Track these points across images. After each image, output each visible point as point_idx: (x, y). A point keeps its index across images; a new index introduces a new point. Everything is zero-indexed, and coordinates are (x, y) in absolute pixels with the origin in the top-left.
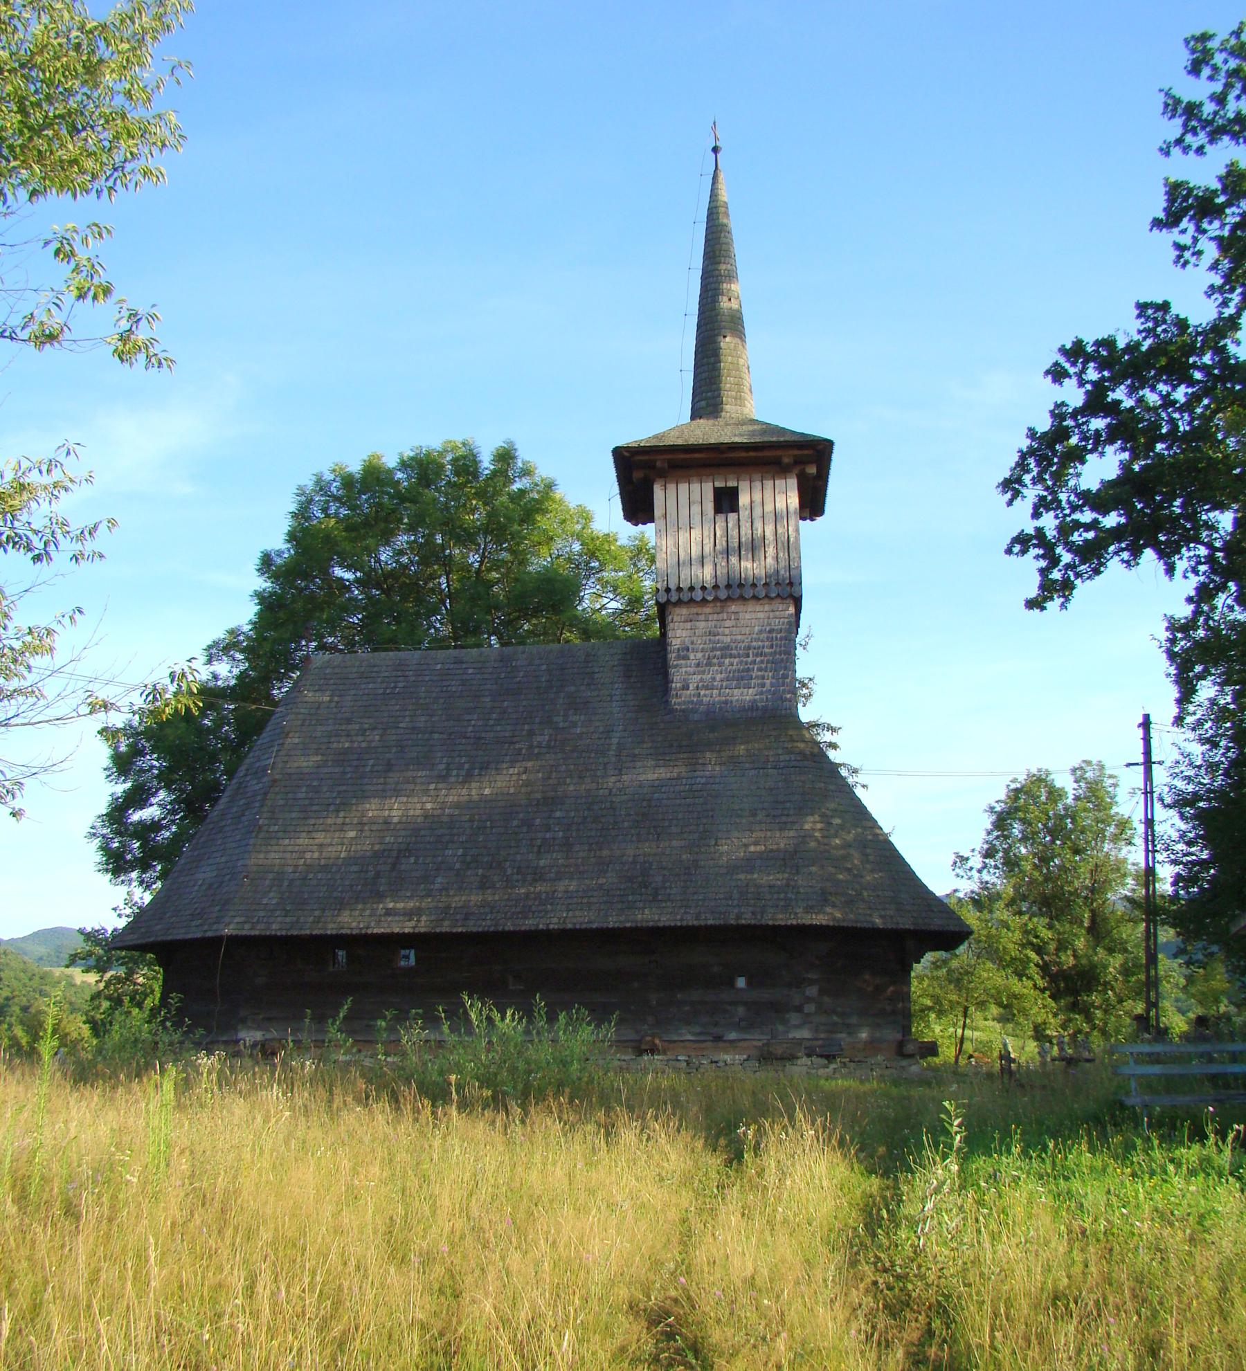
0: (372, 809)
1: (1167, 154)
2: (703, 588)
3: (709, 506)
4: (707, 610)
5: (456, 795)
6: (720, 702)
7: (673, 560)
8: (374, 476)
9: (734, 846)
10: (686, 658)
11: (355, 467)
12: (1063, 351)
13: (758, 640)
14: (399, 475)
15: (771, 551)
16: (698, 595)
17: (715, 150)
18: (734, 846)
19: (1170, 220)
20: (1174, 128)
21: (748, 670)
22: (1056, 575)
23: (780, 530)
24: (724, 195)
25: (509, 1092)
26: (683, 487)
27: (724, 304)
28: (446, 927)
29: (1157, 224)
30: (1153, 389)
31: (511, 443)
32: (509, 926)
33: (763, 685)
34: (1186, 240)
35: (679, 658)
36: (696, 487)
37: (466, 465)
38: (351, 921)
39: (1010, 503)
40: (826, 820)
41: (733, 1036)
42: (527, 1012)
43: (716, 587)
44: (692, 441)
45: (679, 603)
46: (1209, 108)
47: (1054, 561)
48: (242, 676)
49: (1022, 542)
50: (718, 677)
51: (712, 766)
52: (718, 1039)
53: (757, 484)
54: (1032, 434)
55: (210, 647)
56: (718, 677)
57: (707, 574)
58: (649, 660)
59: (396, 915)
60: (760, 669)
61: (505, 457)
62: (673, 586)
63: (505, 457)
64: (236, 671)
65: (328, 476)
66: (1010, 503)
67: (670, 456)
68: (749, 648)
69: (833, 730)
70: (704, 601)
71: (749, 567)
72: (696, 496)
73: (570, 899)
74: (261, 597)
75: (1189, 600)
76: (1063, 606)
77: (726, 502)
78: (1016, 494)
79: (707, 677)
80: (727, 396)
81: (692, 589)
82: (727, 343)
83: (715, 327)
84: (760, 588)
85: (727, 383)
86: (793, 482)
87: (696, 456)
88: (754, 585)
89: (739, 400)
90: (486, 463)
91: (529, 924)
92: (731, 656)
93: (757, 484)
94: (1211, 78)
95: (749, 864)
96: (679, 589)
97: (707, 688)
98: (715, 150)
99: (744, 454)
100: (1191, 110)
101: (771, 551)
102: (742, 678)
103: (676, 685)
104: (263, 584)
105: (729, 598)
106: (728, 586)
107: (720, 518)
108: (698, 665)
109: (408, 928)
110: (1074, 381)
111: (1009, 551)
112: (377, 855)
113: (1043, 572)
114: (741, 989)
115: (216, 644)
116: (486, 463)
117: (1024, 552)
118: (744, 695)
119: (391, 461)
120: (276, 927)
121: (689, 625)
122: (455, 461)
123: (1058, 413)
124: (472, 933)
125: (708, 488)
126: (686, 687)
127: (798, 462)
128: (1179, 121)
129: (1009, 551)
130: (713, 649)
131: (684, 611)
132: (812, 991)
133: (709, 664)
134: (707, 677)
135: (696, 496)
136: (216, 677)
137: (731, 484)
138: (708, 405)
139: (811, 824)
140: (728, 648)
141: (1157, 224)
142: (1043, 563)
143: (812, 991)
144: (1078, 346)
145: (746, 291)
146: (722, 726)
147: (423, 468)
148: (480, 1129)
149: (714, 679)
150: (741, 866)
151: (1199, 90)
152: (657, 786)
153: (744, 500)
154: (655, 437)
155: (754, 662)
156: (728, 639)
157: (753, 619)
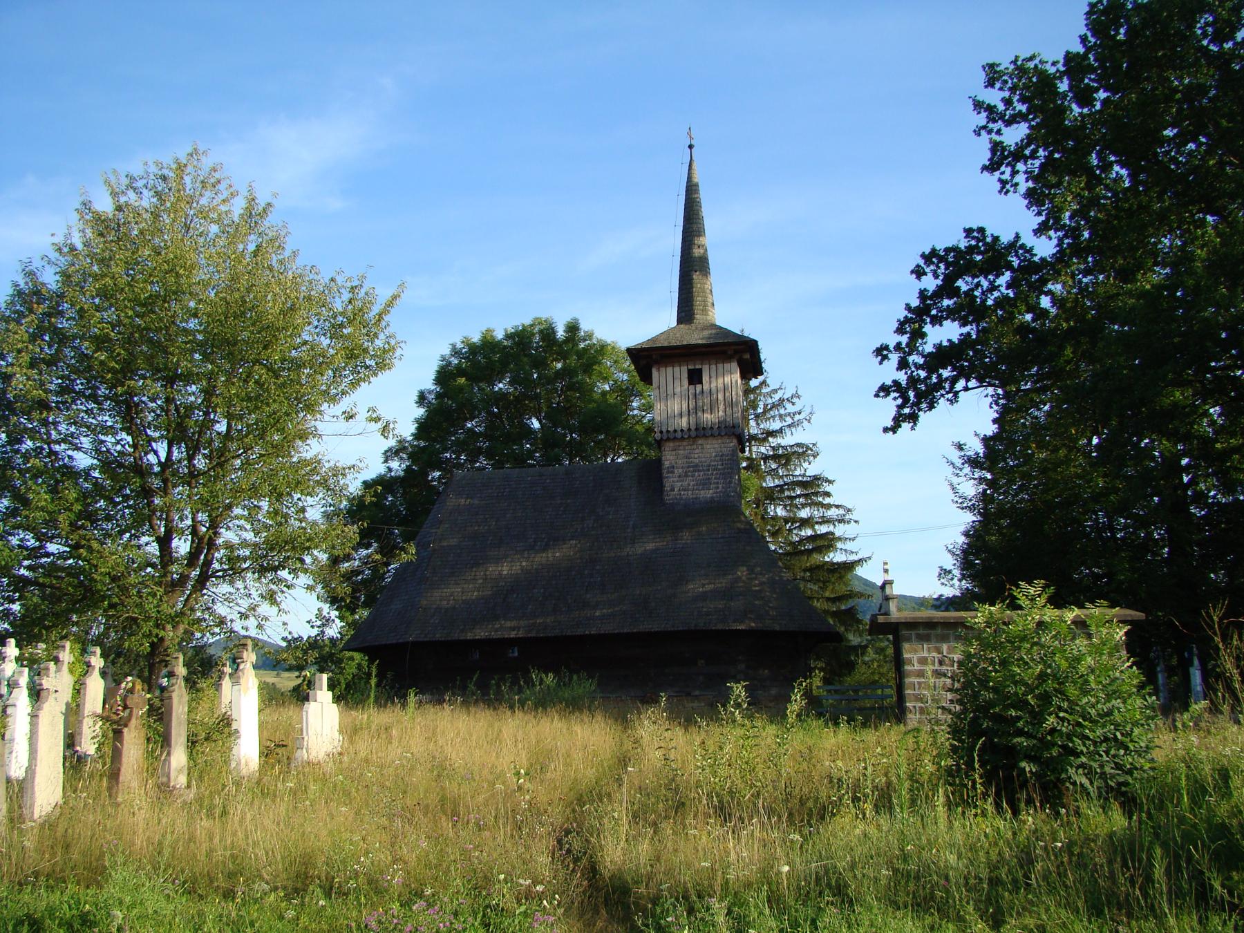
0: (492, 569)
1: (979, 135)
3: (686, 382)
5: (541, 558)
8: (488, 345)
9: (696, 587)
11: (476, 338)
12: (923, 256)
14: (506, 343)
16: (679, 435)
17: (691, 147)
18: (696, 587)
19: (992, 167)
20: (982, 119)
22: (907, 411)
24: (697, 178)
25: (543, 703)
26: (670, 370)
27: (697, 252)
28: (533, 634)
29: (985, 168)
30: (986, 278)
31: (576, 320)
32: (569, 633)
34: (1006, 176)
36: (677, 369)
37: (548, 333)
38: (480, 633)
39: (881, 363)
40: (751, 570)
41: (697, 693)
42: (557, 673)
43: (689, 429)
44: (673, 343)
45: (668, 439)
46: (1001, 107)
47: (906, 400)
48: (408, 470)
49: (884, 390)
51: (686, 537)
52: (688, 694)
53: (713, 367)
54: (908, 308)
55: (386, 452)
58: (652, 473)
59: (508, 628)
61: (573, 328)
63: (573, 328)
64: (404, 466)
65: (459, 346)
66: (881, 363)
69: (830, 482)
70: (683, 439)
71: (708, 418)
72: (677, 374)
73: (602, 615)
75: (995, 421)
76: (912, 428)
77: (695, 378)
78: (885, 357)
79: (685, 484)
80: (698, 309)
81: (675, 431)
82: (696, 276)
83: (692, 266)
85: (698, 301)
86: (734, 365)
89: (705, 312)
90: (561, 333)
91: (579, 632)
93: (713, 367)
94: (1001, 89)
95: (704, 597)
96: (668, 431)
98: (691, 147)
100: (990, 109)
101: (722, 407)
102: (705, 484)
103: (667, 488)
104: (420, 412)
105: (697, 436)
106: (697, 429)
109: (513, 635)
110: (930, 275)
111: (877, 396)
113: (900, 407)
115: (390, 450)
116: (561, 333)
117: (888, 394)
118: (707, 494)
119: (499, 335)
120: (439, 636)
122: (541, 332)
123: (922, 294)
125: (684, 369)
127: (736, 352)
128: (984, 114)
129: (877, 396)
131: (671, 444)
132: (742, 667)
133: (686, 476)
134: (685, 484)
135: (677, 374)
136: (390, 470)
137: (698, 367)
139: (742, 572)
140: (697, 466)
141: (985, 168)
142: (900, 401)
143: (742, 667)
144: (934, 252)
146: (694, 513)
147: (520, 338)
148: (529, 717)
150: (701, 595)
151: (994, 97)
152: (654, 551)
153: (705, 379)
154: (652, 340)
157: (711, 449)
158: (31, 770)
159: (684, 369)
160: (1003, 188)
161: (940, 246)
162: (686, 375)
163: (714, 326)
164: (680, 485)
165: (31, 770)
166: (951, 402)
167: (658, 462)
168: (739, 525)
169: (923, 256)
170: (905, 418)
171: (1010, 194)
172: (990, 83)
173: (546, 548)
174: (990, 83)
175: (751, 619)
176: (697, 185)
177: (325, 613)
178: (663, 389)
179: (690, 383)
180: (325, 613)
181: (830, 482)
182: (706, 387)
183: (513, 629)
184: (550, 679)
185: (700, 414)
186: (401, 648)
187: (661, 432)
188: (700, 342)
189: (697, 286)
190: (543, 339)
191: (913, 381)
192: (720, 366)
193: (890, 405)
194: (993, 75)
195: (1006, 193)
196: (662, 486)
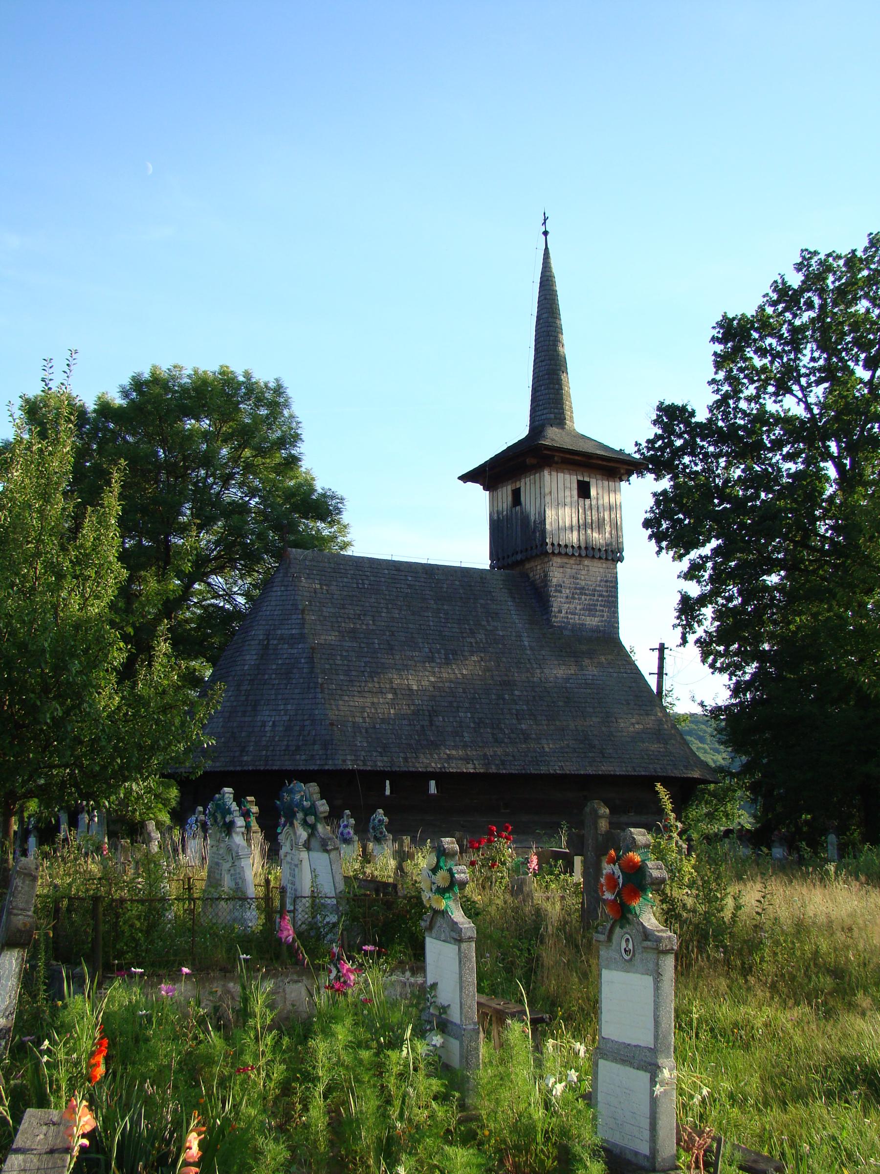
2: (572, 546)
3: (575, 493)
4: (572, 561)
5: (446, 674)
6: (580, 624)
7: (555, 526)
10: (560, 592)
13: (600, 586)
15: (608, 529)
16: (563, 551)
17: (546, 233)
21: (595, 605)
23: (613, 516)
26: (561, 475)
33: (603, 616)
35: (556, 591)
43: (579, 547)
50: (578, 607)
56: (578, 607)
57: (573, 538)
60: (601, 606)
62: (556, 543)
67: (562, 455)
68: (595, 590)
74: (323, 508)
77: (584, 491)
79: (572, 606)
81: (566, 546)
84: (603, 552)
87: (576, 458)
88: (600, 550)
92: (585, 594)
96: (559, 545)
97: (572, 614)
98: (546, 233)
99: (600, 462)
101: (608, 529)
103: (555, 609)
106: (586, 548)
107: (581, 501)
108: (567, 597)
112: (416, 713)
114: (812, 818)
118: (592, 622)
121: (561, 570)
124: (512, 774)
125: (574, 479)
126: (560, 612)
130: (576, 588)
133: (573, 598)
137: (587, 479)
138: (556, 418)
140: (583, 588)
145: (571, 346)
149: (576, 608)
155: (597, 600)
156: (583, 583)
157: (596, 569)
158: (538, 1048)
159: (574, 479)
162: (575, 485)
165: (538, 1048)
178: (554, 495)
179: (579, 496)
182: (594, 502)
187: (553, 544)
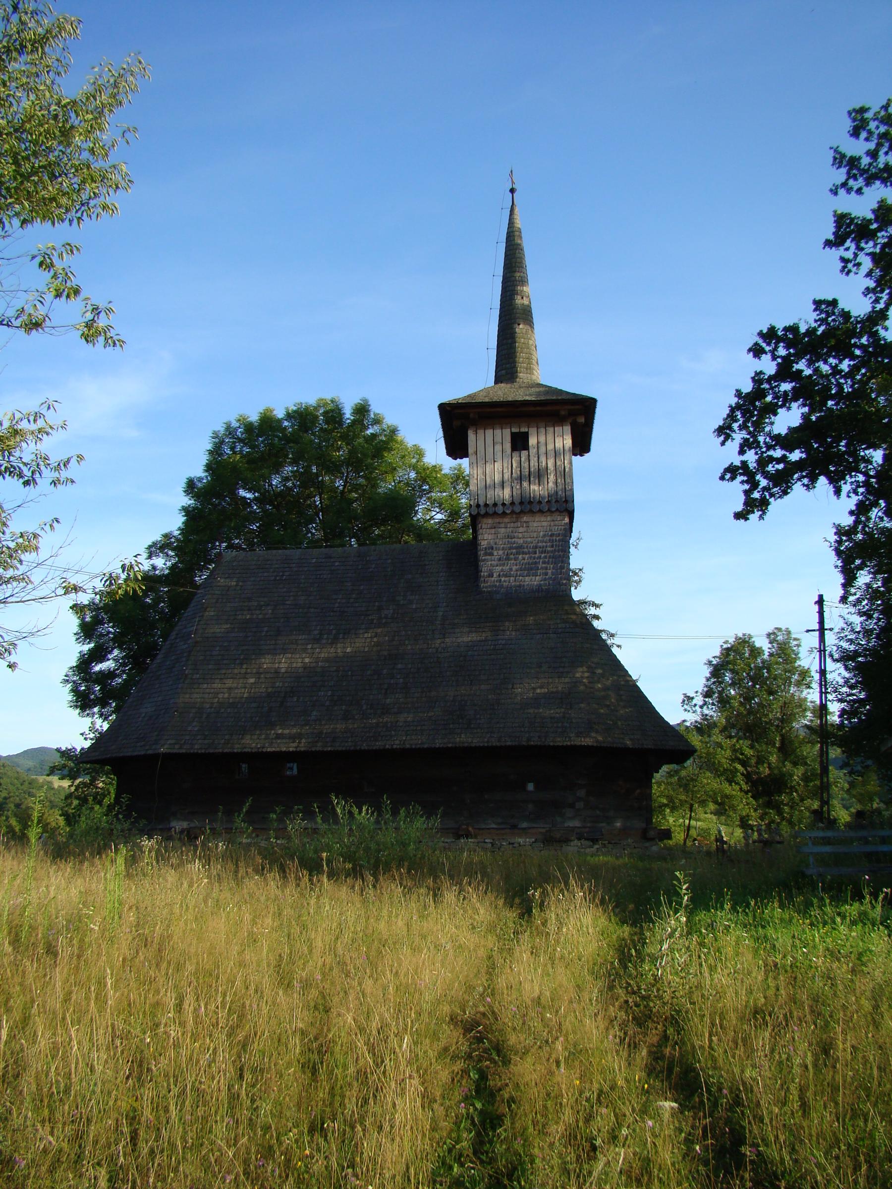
0: (266, 662)
1: (836, 194)
5: (326, 653)
8: (268, 423)
9: (525, 689)
11: (254, 417)
12: (761, 334)
16: (500, 509)
17: (512, 191)
18: (525, 689)
19: (836, 242)
20: (840, 175)
22: (756, 495)
24: (519, 223)
25: (365, 865)
26: (489, 432)
28: (319, 747)
29: (828, 244)
30: (826, 362)
32: (365, 746)
34: (849, 255)
36: (498, 432)
37: (334, 414)
38: (251, 743)
39: (723, 444)
40: (591, 670)
41: (524, 825)
42: (377, 808)
43: (513, 503)
44: (495, 399)
45: (487, 515)
46: (865, 161)
47: (754, 485)
48: (173, 568)
49: (731, 472)
51: (509, 632)
52: (514, 827)
53: (542, 430)
54: (738, 394)
55: (150, 547)
59: (284, 738)
61: (362, 410)
63: (362, 410)
64: (169, 564)
65: (235, 424)
66: (723, 444)
69: (597, 606)
72: (498, 438)
73: (408, 728)
75: (851, 513)
76: (761, 517)
77: (520, 443)
79: (506, 568)
80: (521, 367)
81: (495, 505)
82: (521, 328)
83: (512, 317)
85: (521, 357)
86: (567, 429)
89: (529, 370)
90: (348, 414)
91: (378, 745)
93: (542, 430)
94: (867, 139)
96: (486, 505)
98: (512, 191)
100: (853, 163)
101: (552, 478)
102: (531, 569)
106: (521, 503)
111: (722, 478)
113: (747, 493)
115: (154, 544)
116: (348, 414)
117: (733, 478)
118: (533, 581)
119: (280, 414)
120: (198, 747)
122: (325, 413)
123: (758, 378)
125: (507, 433)
128: (844, 170)
129: (722, 478)
131: (490, 521)
132: (582, 793)
133: (508, 559)
134: (506, 568)
135: (498, 438)
136: (154, 568)
137: (523, 430)
139: (581, 673)
140: (521, 547)
141: (828, 244)
143: (582, 793)
144: (772, 330)
146: (518, 603)
147: (303, 417)
151: (858, 148)
154: (469, 396)
160: (844, 267)
161: (780, 325)
163: (540, 385)
164: (498, 570)
166: (807, 487)
167: (474, 542)
168: (574, 617)
169: (761, 334)
170: (754, 506)
171: (851, 274)
172: (855, 133)
173: (334, 641)
174: (855, 133)
175: (597, 732)
176: (520, 231)
177: (98, 726)
180: (98, 726)
181: (597, 606)
183: (293, 738)
184: (364, 815)
185: (525, 484)
186: (151, 760)
188: (528, 398)
189: (520, 341)
190: (327, 422)
191: (762, 462)
192: (550, 430)
193: (736, 490)
194: (859, 124)
195: (848, 273)
196: (477, 570)
